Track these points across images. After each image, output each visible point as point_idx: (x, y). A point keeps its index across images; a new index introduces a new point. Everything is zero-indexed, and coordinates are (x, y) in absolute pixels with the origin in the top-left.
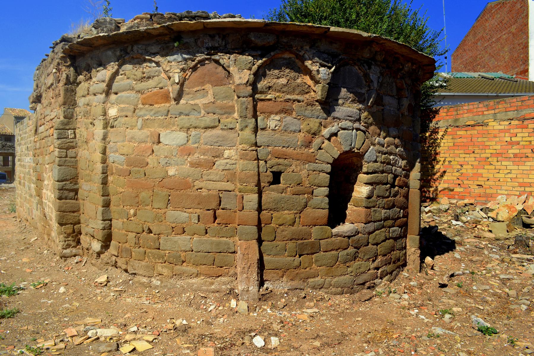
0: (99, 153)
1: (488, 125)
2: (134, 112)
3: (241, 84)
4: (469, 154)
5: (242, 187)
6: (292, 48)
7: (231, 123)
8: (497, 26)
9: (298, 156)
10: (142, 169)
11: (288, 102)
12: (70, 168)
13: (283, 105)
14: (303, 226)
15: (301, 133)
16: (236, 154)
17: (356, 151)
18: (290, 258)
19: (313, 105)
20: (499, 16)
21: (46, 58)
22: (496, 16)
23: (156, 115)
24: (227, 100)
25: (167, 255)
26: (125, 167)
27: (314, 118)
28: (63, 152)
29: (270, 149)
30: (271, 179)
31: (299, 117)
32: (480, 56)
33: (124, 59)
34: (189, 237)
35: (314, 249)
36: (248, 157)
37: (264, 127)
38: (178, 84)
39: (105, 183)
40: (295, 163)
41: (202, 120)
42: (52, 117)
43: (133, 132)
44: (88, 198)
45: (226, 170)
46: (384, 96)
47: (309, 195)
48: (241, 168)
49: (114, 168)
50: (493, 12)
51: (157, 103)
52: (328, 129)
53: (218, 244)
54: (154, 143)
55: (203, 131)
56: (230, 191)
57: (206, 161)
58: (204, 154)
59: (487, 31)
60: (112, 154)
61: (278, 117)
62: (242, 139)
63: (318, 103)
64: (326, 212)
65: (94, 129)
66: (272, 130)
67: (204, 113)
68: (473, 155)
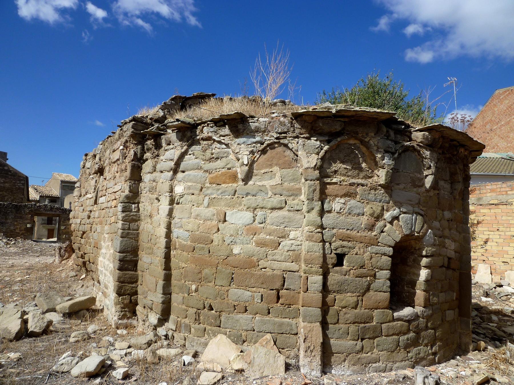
0: (163, 228)
1: (512, 204)
2: (201, 190)
3: (309, 168)
4: (494, 231)
5: (307, 268)
6: (358, 134)
7: (298, 205)
8: (505, 110)
9: (361, 239)
10: (206, 246)
11: (352, 185)
12: (131, 241)
13: (347, 189)
14: (365, 309)
15: (364, 216)
16: (302, 236)
17: (416, 234)
18: (352, 342)
19: (376, 189)
20: (507, 102)
21: (112, 135)
22: (505, 101)
23: (223, 195)
24: (295, 182)
25: (228, 333)
26: (189, 243)
27: (377, 201)
28: (126, 224)
29: (335, 231)
30: (334, 261)
31: (362, 201)
32: (489, 137)
33: (194, 140)
34: (251, 316)
35: (377, 333)
36: (314, 239)
37: (330, 209)
38: (247, 165)
39: (167, 257)
40: (358, 245)
41: (268, 201)
42: (115, 190)
43: (199, 210)
44: (148, 270)
45: (291, 250)
46: (439, 181)
47: (372, 278)
48: (306, 249)
49: (177, 244)
50: (501, 98)
51: (224, 183)
52: (391, 212)
53: (281, 325)
54: (220, 221)
55: (270, 211)
56: (295, 272)
57: (271, 241)
58: (270, 235)
59: (495, 115)
60: (176, 230)
61: (342, 200)
62: (308, 221)
63: (380, 187)
64: (388, 295)
65: (159, 204)
66: (337, 212)
67: (271, 194)
68: (497, 233)
